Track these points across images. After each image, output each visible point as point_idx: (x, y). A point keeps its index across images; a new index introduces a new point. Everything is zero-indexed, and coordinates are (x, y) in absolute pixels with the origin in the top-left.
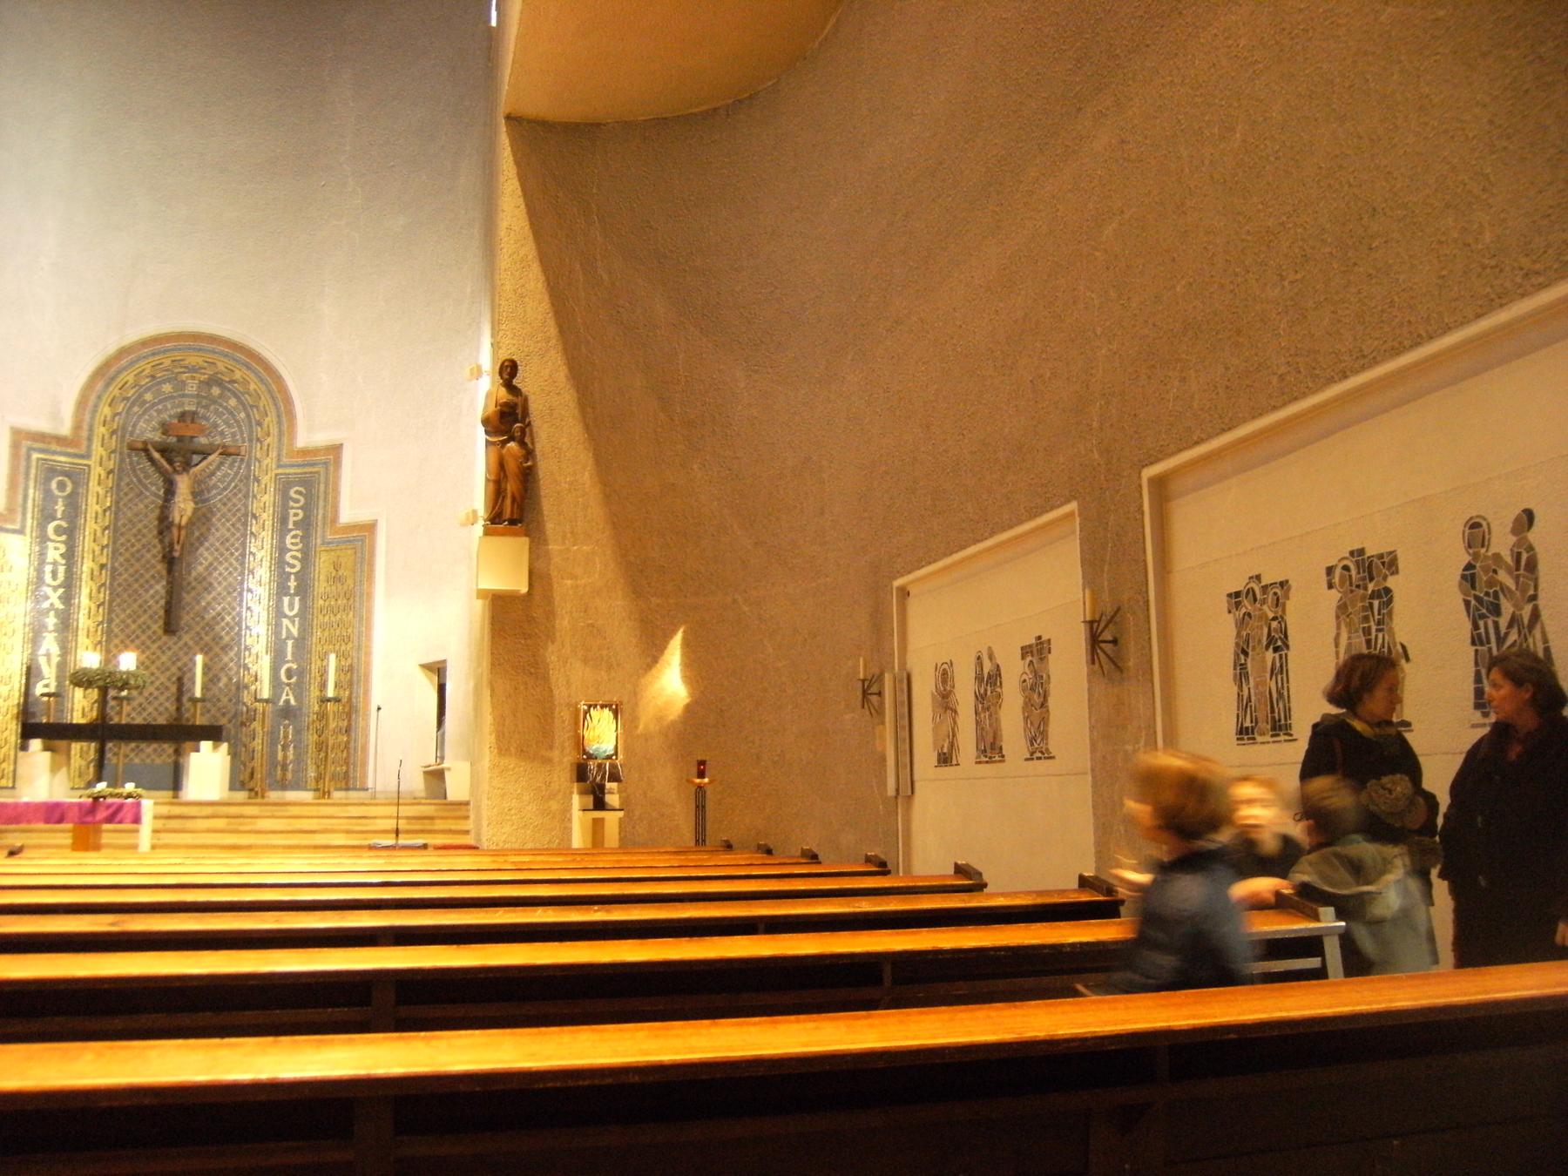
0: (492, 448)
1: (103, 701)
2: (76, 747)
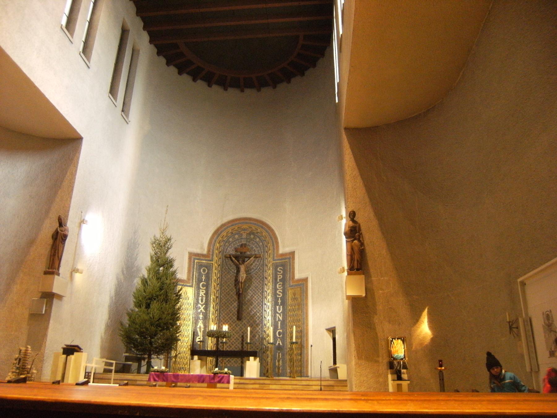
1: (217, 344)
2: (209, 359)
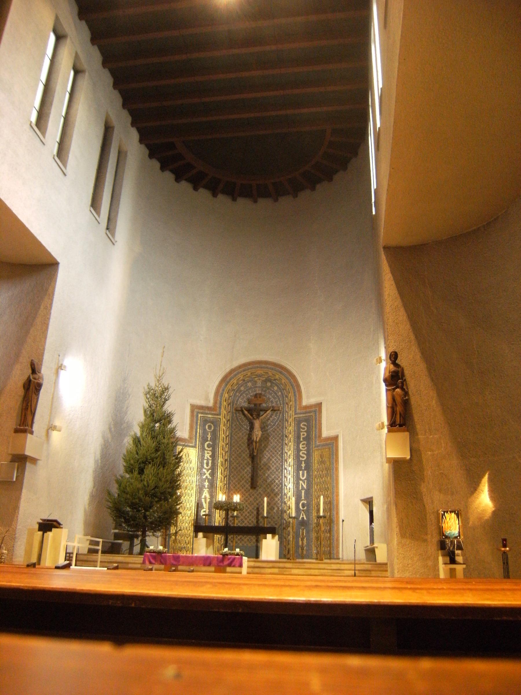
0: (390, 393)
1: (227, 518)
2: (217, 537)
